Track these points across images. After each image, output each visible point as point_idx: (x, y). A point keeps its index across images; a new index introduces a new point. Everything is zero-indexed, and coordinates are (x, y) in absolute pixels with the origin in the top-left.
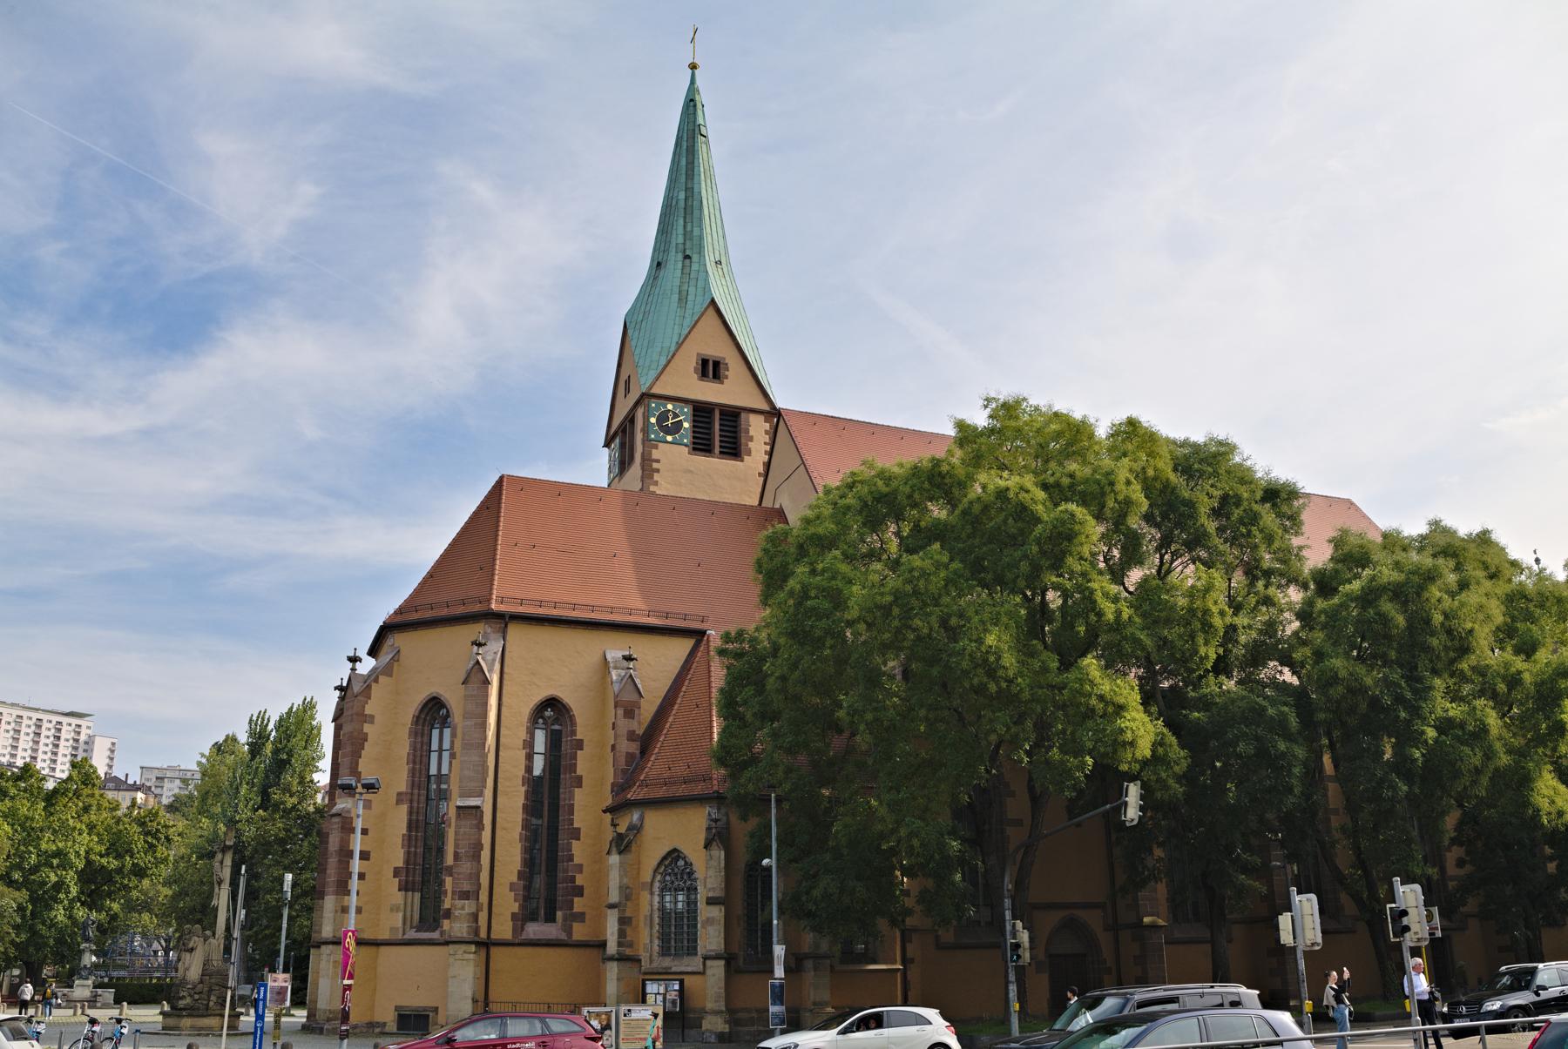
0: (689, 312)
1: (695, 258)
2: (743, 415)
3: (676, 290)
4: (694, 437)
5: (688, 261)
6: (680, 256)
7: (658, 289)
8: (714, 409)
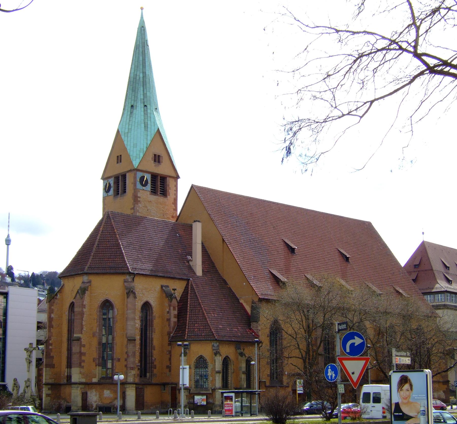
0: (149, 133)
1: (148, 106)
2: (168, 178)
3: (143, 121)
4: (152, 187)
5: (145, 108)
6: (142, 105)
7: (134, 119)
8: (158, 176)
